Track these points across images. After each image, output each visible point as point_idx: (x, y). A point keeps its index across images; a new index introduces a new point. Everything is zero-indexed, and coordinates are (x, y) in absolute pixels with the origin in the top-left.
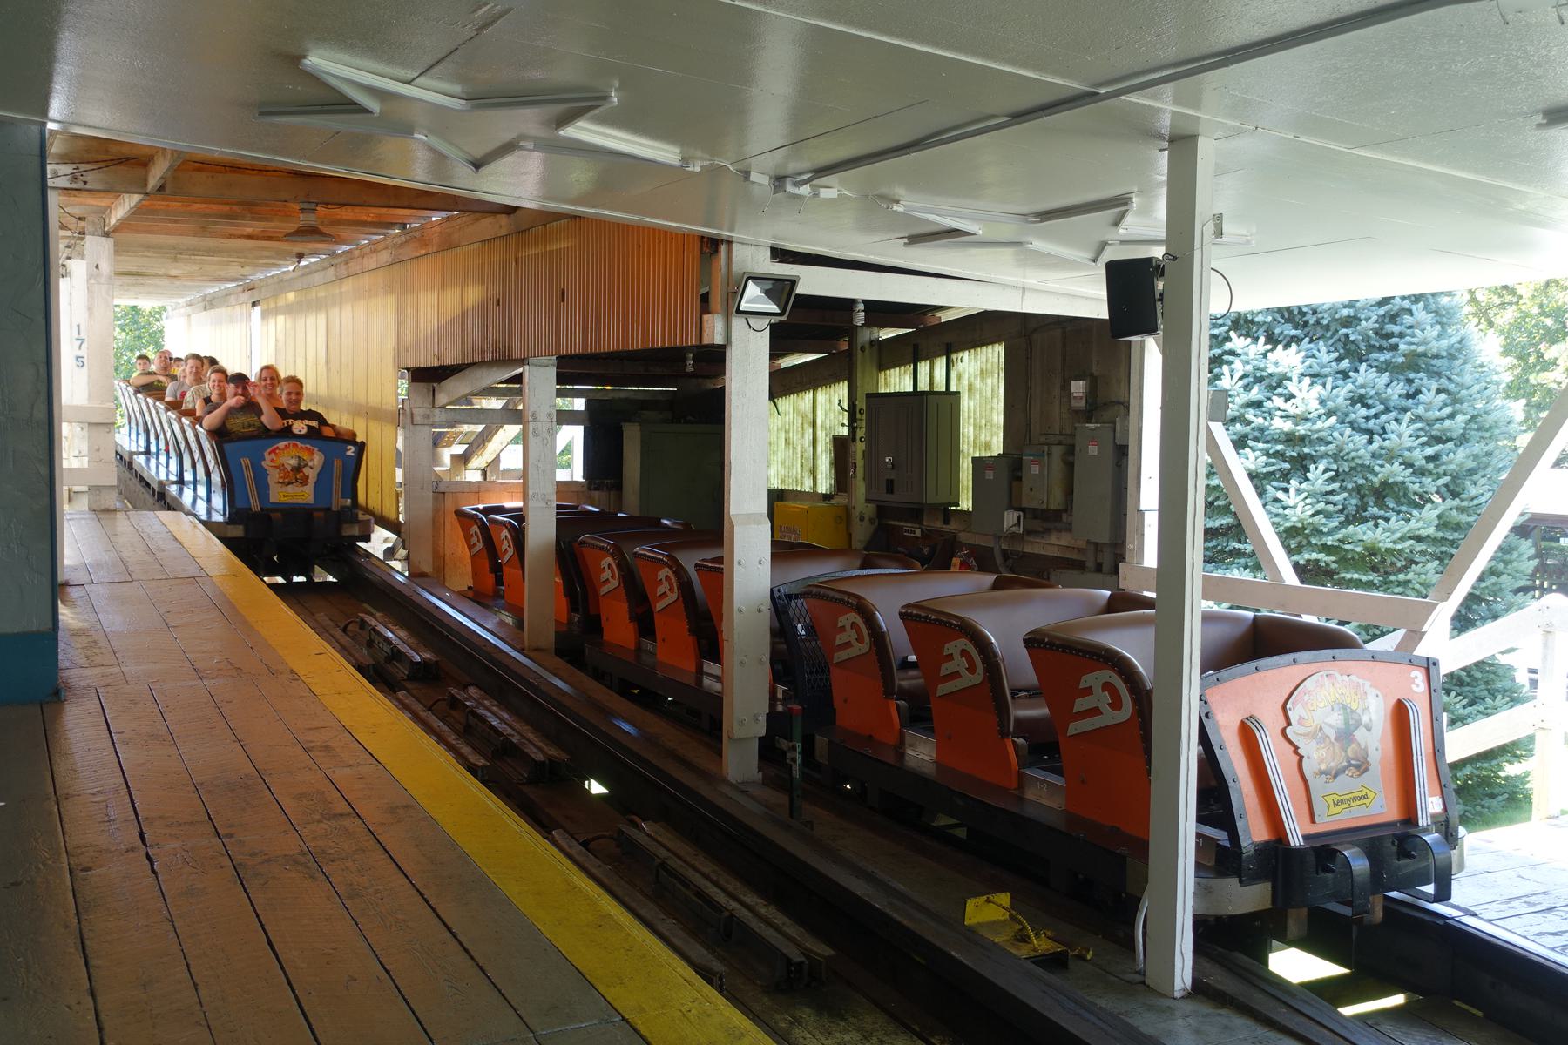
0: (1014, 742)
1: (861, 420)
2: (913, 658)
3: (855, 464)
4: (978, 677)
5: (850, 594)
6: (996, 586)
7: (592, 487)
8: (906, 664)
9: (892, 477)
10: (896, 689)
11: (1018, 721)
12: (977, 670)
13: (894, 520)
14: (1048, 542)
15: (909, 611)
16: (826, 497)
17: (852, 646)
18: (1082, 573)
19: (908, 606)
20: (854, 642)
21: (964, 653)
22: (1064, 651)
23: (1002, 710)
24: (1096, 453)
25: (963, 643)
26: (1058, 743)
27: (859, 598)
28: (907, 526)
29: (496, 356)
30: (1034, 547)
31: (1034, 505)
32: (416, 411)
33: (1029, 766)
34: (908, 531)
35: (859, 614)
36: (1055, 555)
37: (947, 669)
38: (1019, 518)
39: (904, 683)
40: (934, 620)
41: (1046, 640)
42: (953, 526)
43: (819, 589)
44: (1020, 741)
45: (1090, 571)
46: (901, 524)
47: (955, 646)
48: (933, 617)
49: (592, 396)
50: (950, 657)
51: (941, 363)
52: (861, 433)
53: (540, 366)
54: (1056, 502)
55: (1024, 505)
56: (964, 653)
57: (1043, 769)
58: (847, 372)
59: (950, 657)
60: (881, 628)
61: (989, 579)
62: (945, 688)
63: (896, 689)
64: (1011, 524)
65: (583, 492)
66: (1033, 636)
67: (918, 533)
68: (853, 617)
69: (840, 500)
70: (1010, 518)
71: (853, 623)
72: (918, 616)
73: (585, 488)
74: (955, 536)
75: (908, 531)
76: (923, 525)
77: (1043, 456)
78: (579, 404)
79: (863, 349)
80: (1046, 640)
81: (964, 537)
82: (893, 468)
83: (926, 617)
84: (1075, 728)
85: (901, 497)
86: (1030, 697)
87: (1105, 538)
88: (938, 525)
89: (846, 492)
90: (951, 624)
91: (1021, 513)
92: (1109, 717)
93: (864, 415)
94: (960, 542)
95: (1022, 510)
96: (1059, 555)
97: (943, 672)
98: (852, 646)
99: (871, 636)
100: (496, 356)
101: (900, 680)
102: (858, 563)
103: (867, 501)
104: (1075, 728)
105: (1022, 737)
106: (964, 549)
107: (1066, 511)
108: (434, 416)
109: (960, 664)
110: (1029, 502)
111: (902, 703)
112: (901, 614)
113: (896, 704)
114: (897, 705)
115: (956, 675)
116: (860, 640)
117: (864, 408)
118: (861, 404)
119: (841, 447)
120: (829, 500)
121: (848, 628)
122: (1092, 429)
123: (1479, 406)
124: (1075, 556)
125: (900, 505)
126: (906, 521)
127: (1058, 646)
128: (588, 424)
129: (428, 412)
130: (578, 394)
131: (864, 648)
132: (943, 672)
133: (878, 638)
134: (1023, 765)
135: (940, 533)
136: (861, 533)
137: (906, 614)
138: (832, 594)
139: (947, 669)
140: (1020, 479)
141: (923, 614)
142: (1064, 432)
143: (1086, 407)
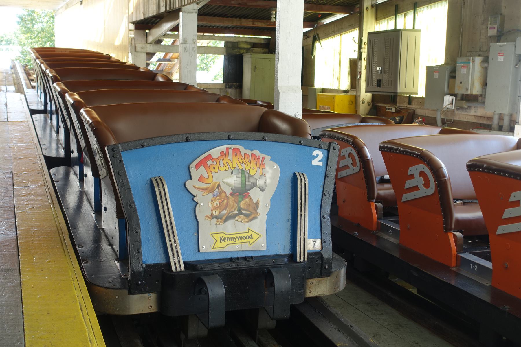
0: (454, 235)
1: (365, 48)
2: (387, 177)
3: (361, 72)
4: (432, 190)
5: (348, 135)
6: (442, 132)
7: (227, 87)
8: (383, 181)
9: (381, 78)
10: (376, 196)
11: (458, 221)
12: (431, 186)
13: (381, 103)
14: (469, 114)
15: (386, 145)
16: (345, 92)
17: (419, 189)
18: (490, 131)
19: (384, 143)
20: (350, 166)
21: (422, 174)
22: (499, 174)
23: (447, 212)
24: (502, 60)
25: (422, 167)
26: (488, 236)
27: (353, 137)
28: (388, 106)
29: (167, 9)
30: (462, 116)
31: (463, 92)
32: (137, 45)
33: (465, 251)
34: (388, 109)
35: (354, 148)
36: (473, 121)
37: (409, 184)
38: (452, 100)
39: (382, 192)
40: (402, 151)
41: (485, 165)
42: (414, 106)
43: (330, 133)
44: (459, 234)
45: (495, 130)
46: (385, 105)
47: (416, 169)
48: (402, 149)
49: (228, 40)
50: (412, 176)
51: (410, 14)
52: (364, 55)
53: (188, 13)
54: (476, 90)
55: (456, 92)
56: (422, 174)
57: (474, 254)
58: (358, 24)
59: (412, 176)
60: (367, 157)
61: (438, 130)
62: (407, 197)
63: (376, 196)
64: (447, 104)
65: (223, 89)
66: (475, 163)
67: (394, 110)
68: (350, 149)
69: (353, 93)
70: (448, 99)
71: (350, 153)
72: (391, 148)
73: (224, 87)
74: (414, 111)
75: (388, 109)
76: (396, 105)
77: (470, 63)
78: (222, 44)
79: (367, 8)
80: (485, 165)
81: (419, 112)
82: (381, 73)
83: (397, 150)
84: (502, 229)
85: (385, 89)
86: (464, 204)
87: (506, 111)
88: (405, 105)
89: (355, 89)
90: (414, 154)
91: (454, 98)
92: (424, 192)
93: (366, 46)
94: (417, 115)
95: (455, 95)
96: (475, 121)
97: (407, 186)
98: (419, 189)
99: (361, 161)
100: (167, 9)
101: (378, 190)
102: (358, 121)
103: (367, 91)
104: (502, 229)
105: (459, 232)
106: (419, 118)
107: (481, 95)
108: (147, 48)
109: (419, 181)
110: (460, 91)
111: (379, 204)
112: (380, 148)
113: (375, 204)
114: (376, 206)
115: (416, 188)
116: (354, 164)
117: (367, 42)
118: (365, 39)
119: (354, 65)
120: (346, 93)
121: (347, 156)
122: (500, 46)
123: (109, 300)
124: (485, 122)
125: (385, 94)
126: (387, 103)
127: (494, 170)
128: (225, 54)
129: (144, 45)
130: (221, 39)
131: (357, 169)
132: (407, 186)
133: (365, 163)
134: (460, 249)
135: (407, 110)
136: (363, 109)
137: (383, 147)
138: (337, 135)
139: (409, 184)
140: (454, 78)
141: (395, 147)
142: (482, 50)
143: (497, 33)
